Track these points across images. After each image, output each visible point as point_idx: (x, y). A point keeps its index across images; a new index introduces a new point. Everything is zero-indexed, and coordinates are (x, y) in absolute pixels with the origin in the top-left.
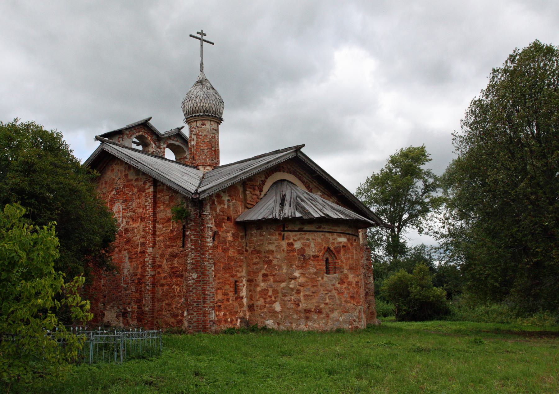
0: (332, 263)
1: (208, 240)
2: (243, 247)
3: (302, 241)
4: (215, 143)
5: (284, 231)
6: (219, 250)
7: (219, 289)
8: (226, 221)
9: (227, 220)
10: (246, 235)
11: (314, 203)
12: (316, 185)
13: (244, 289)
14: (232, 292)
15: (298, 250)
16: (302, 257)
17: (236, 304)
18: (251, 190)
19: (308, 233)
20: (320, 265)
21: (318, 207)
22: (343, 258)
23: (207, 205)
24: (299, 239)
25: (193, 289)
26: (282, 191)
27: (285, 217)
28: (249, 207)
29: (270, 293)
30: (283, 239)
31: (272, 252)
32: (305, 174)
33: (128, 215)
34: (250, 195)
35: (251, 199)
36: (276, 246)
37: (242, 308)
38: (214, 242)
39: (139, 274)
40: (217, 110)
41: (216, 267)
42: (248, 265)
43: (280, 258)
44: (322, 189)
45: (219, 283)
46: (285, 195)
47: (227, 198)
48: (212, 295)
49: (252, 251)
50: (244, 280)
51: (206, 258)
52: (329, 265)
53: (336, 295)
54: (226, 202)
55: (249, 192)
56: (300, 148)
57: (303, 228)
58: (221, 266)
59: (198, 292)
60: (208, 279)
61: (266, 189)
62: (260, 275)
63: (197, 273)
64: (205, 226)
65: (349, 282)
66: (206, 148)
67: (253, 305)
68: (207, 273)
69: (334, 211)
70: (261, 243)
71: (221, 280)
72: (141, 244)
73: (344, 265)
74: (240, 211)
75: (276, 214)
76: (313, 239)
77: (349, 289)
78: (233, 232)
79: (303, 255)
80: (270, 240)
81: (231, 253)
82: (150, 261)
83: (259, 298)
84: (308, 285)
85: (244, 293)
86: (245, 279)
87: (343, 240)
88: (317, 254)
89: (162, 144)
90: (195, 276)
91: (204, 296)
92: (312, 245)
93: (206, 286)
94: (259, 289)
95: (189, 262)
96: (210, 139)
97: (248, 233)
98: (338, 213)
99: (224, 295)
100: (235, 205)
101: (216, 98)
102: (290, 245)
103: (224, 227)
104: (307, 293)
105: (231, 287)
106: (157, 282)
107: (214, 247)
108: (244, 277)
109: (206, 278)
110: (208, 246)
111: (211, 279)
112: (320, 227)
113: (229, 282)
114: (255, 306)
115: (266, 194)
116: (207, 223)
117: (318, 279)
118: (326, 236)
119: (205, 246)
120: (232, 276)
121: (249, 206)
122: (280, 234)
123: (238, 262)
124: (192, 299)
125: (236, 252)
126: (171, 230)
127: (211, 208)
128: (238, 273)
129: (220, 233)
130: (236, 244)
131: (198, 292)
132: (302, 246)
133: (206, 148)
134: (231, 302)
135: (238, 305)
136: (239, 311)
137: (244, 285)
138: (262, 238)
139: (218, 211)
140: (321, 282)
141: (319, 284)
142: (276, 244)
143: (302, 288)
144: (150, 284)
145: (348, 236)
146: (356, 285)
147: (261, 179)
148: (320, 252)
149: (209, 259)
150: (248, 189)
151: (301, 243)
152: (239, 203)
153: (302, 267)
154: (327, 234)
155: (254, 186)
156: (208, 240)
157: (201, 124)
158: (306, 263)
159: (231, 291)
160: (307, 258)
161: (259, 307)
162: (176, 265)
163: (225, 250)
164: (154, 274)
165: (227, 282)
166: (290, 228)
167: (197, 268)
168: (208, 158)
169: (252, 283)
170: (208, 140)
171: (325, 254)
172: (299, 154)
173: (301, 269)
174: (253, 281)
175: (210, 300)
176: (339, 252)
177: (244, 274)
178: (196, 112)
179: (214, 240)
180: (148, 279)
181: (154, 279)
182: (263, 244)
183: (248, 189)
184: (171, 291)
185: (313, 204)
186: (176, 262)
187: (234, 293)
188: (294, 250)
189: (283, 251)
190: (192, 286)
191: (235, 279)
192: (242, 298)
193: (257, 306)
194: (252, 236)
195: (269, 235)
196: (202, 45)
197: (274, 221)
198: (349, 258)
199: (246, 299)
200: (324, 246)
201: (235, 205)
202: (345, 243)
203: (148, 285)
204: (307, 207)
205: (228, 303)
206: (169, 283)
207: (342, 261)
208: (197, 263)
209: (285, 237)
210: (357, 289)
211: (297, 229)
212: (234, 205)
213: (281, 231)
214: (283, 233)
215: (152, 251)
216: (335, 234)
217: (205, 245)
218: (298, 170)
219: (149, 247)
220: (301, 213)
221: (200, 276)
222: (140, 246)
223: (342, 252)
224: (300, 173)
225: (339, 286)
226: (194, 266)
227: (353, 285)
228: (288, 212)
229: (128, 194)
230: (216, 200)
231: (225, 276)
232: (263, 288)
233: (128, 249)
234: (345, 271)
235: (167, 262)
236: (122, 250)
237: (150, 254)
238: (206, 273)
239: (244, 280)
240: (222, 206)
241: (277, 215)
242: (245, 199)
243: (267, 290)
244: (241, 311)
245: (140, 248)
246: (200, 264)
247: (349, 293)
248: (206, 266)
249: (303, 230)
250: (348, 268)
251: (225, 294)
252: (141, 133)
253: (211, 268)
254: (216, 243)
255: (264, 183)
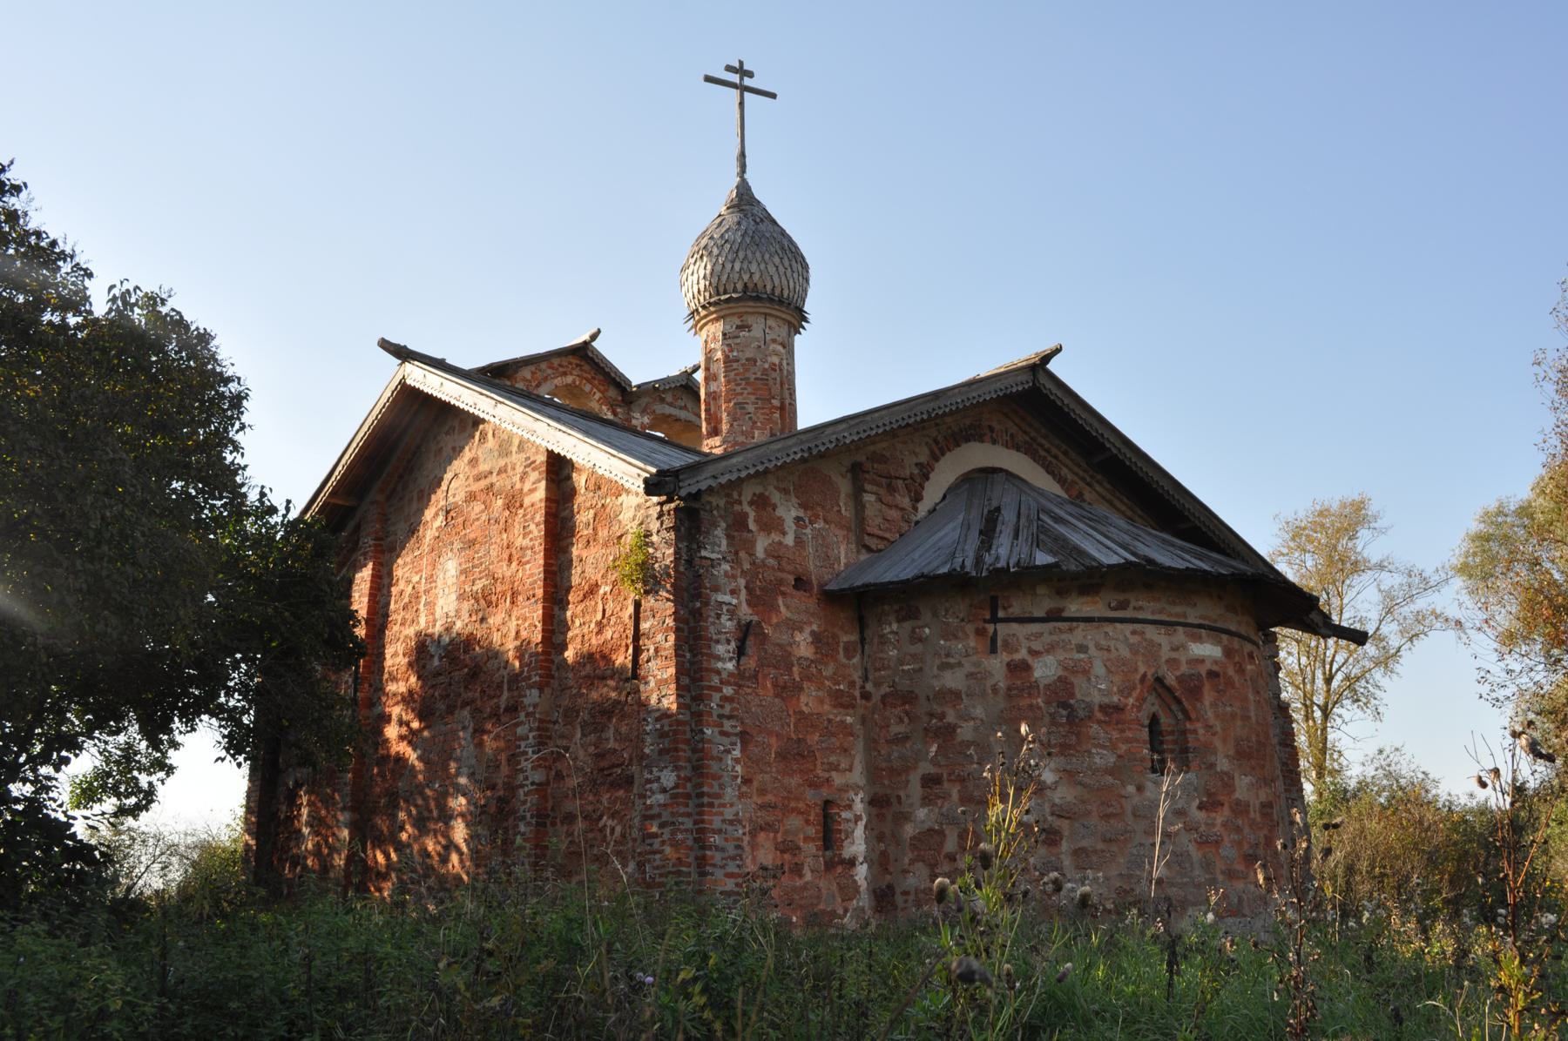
0: (1172, 733)
1: (720, 649)
2: (852, 684)
3: (1062, 655)
4: (782, 384)
5: (995, 620)
6: (765, 687)
7: (762, 829)
8: (790, 590)
9: (796, 587)
10: (863, 641)
11: (1103, 529)
12: (1104, 493)
13: (859, 832)
14: (813, 840)
15: (1047, 687)
16: (1064, 713)
17: (827, 885)
18: (882, 491)
19: (1082, 625)
20: (1128, 741)
21: (1115, 537)
22: (1210, 714)
23: (715, 525)
24: (1051, 649)
25: (662, 826)
26: (990, 499)
27: (999, 566)
28: (873, 547)
29: (950, 845)
30: (993, 650)
31: (956, 695)
32: (1065, 453)
33: (475, 588)
34: (878, 505)
35: (879, 520)
36: (970, 675)
37: (851, 899)
38: (744, 660)
39: (500, 785)
40: (784, 282)
41: (753, 749)
42: (871, 745)
43: (983, 716)
44: (1123, 508)
45: (761, 807)
46: (998, 509)
47: (794, 513)
48: (732, 852)
49: (884, 697)
50: (858, 799)
51: (710, 714)
52: (1162, 743)
53: (1192, 848)
54: (790, 526)
55: (872, 498)
56: (1047, 358)
57: (1062, 610)
58: (769, 745)
59: (680, 836)
60: (716, 789)
61: (933, 492)
62: (915, 779)
63: (677, 768)
64: (708, 597)
65: (1238, 803)
66: (753, 398)
67: (890, 887)
68: (714, 767)
69: (1172, 549)
70: (917, 666)
71: (770, 798)
72: (509, 682)
73: (1218, 743)
74: (843, 561)
75: (966, 559)
76: (1099, 647)
77: (1238, 830)
78: (815, 627)
79: (1065, 705)
80: (947, 655)
81: (809, 701)
82: (531, 735)
83: (912, 862)
84: (1088, 813)
85: (857, 845)
86: (861, 795)
87: (1208, 650)
88: (1115, 699)
89: (637, 415)
90: (669, 778)
91: (700, 853)
92: (1099, 669)
93: (711, 814)
94: (909, 830)
95: (648, 728)
96: (765, 370)
97: (868, 633)
98: (1187, 557)
99: (783, 852)
100: (824, 538)
101: (783, 248)
102: (1019, 669)
103: (783, 609)
104: (1084, 843)
105: (807, 822)
106: (553, 809)
107: (739, 679)
108: (856, 788)
109: (711, 786)
110: (718, 672)
111: (729, 790)
112: (1123, 606)
113: (801, 805)
114: (898, 890)
115: (935, 510)
116: (716, 589)
117: (1123, 793)
118: (1148, 636)
119: (707, 670)
120: (814, 785)
121: (873, 543)
122: (980, 633)
123: (833, 735)
124: (658, 863)
125: (827, 700)
126: (599, 624)
127: (729, 537)
128: (834, 774)
129: (768, 630)
130: (828, 671)
131: (680, 836)
132: (1060, 672)
133: (753, 398)
134: (808, 876)
135: (834, 887)
136: (841, 912)
137: (858, 818)
138: (918, 648)
139: (760, 552)
140: (1136, 799)
141: (1129, 809)
142: (968, 668)
143: (1064, 825)
144: (528, 815)
145: (1224, 637)
146: (1264, 815)
147: (915, 460)
148: (1129, 695)
149: (721, 716)
150: (868, 487)
151: (1059, 663)
152: (841, 533)
153: (1065, 749)
154: (1151, 632)
155: (889, 477)
156: (720, 649)
157: (738, 327)
158: (1078, 735)
159: (807, 839)
160: (1081, 714)
161: (911, 897)
162: (612, 744)
163: (786, 691)
164: (543, 779)
165: (793, 804)
166: (1016, 610)
167: (676, 750)
168: (758, 428)
169: (884, 811)
170: (759, 375)
171: (1144, 700)
172: (1043, 380)
173: (1061, 753)
174: (889, 804)
175: (723, 867)
176: (1195, 692)
177: (857, 776)
178: (721, 290)
179: (741, 652)
180: (526, 801)
181: (544, 797)
182: (921, 669)
183: (868, 487)
184: (595, 839)
185: (1095, 530)
186: (610, 733)
187: (820, 843)
188: (1033, 687)
189: (995, 690)
190: (659, 816)
191: (825, 793)
192: (852, 863)
193: (906, 893)
194: (883, 643)
195: (943, 638)
196: (741, 104)
197: (956, 584)
198: (1233, 716)
199: (865, 866)
200: (1142, 670)
201: (824, 538)
202: (1216, 662)
203: (524, 818)
204: (1075, 538)
205: (799, 883)
206: (590, 808)
207: (1208, 727)
208: (676, 732)
209: (999, 643)
210: (1265, 831)
211: (1041, 614)
212: (818, 535)
213: (985, 621)
214: (990, 628)
215: (537, 700)
216: (1180, 629)
217: (705, 665)
218: (1043, 441)
219: (530, 687)
220: (1051, 552)
221: (689, 779)
222: (505, 687)
223: (1208, 696)
224: (1048, 451)
225: (1200, 816)
226: (666, 741)
227: (1252, 815)
228: (1005, 551)
229: (478, 519)
230: (752, 515)
231: (786, 780)
232: (927, 826)
233: (473, 701)
234: (1223, 764)
235: (584, 735)
236: (455, 706)
237: (531, 709)
238: (708, 766)
239: (858, 799)
240: (775, 537)
241: (969, 564)
242: (860, 519)
243: (941, 833)
244: (846, 911)
245: (506, 695)
246: (688, 736)
247: (1239, 844)
248: (709, 741)
249: (1065, 614)
250: (1231, 752)
251: (788, 847)
252: (569, 379)
253: (728, 752)
254: (750, 663)
255: (925, 472)
